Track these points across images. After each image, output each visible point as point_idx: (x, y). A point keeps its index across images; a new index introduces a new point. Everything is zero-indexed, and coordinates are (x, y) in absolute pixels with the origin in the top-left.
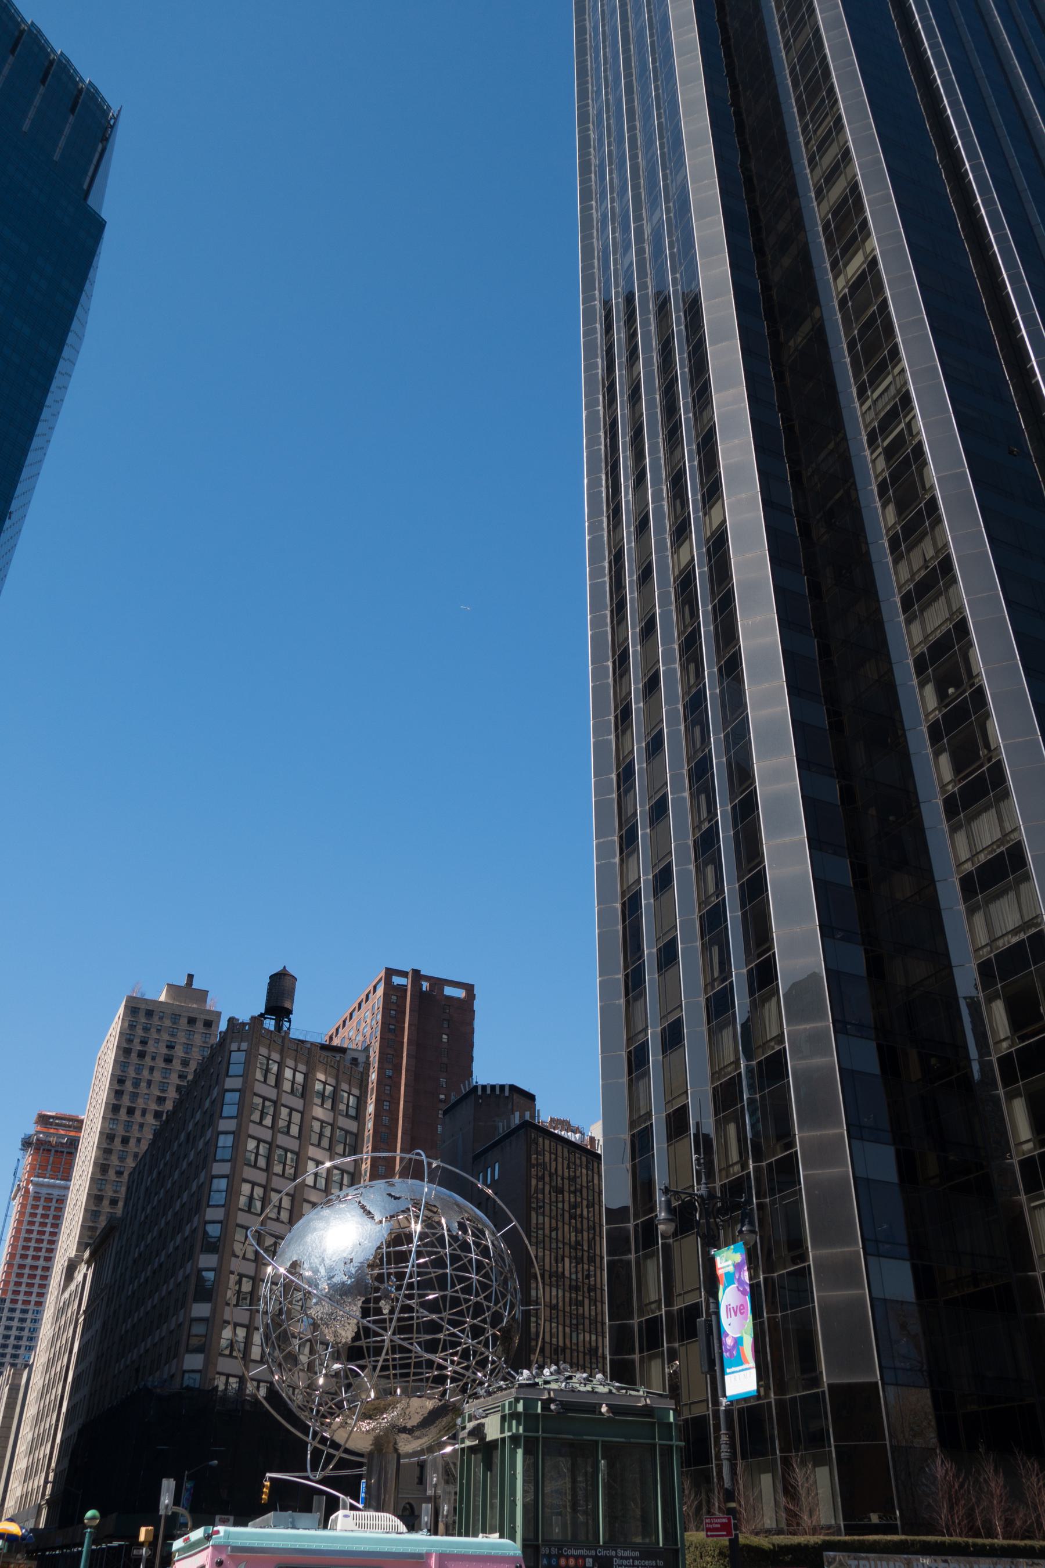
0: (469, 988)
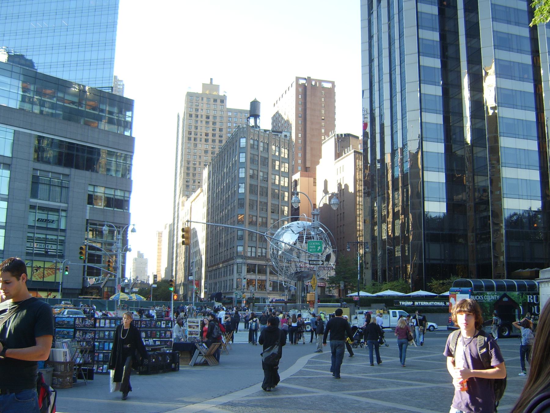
0: (333, 83)
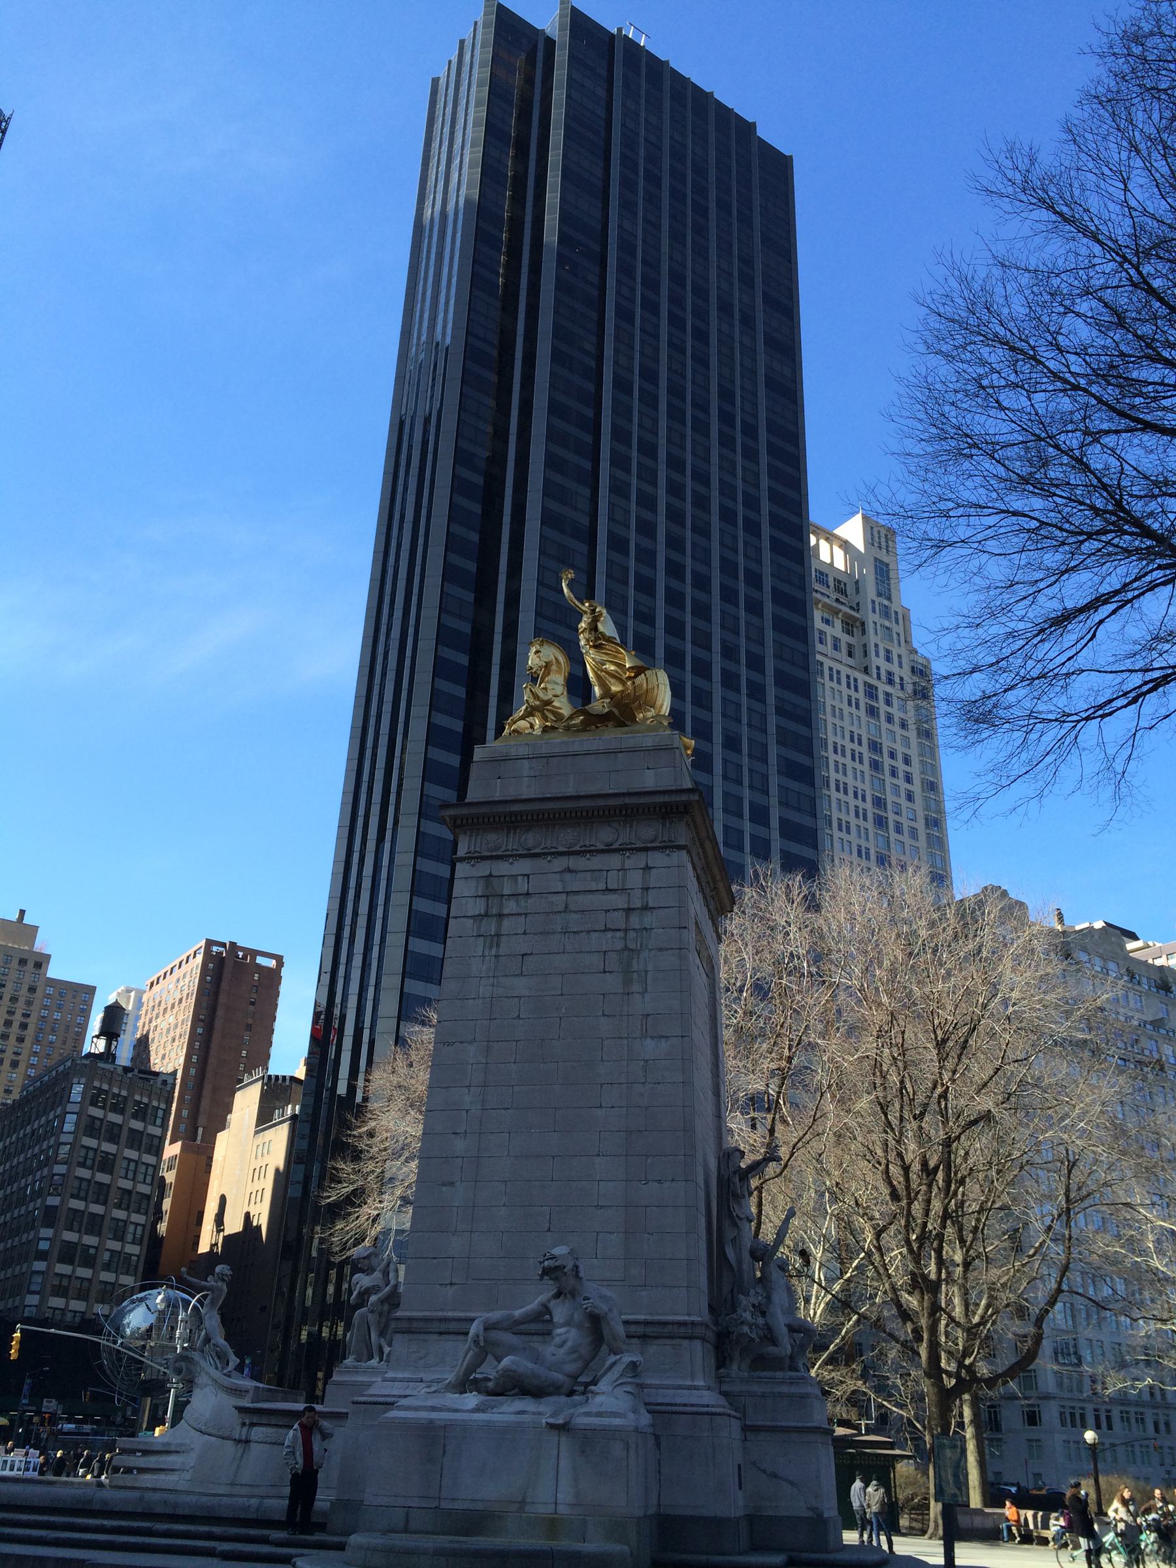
0: (279, 960)
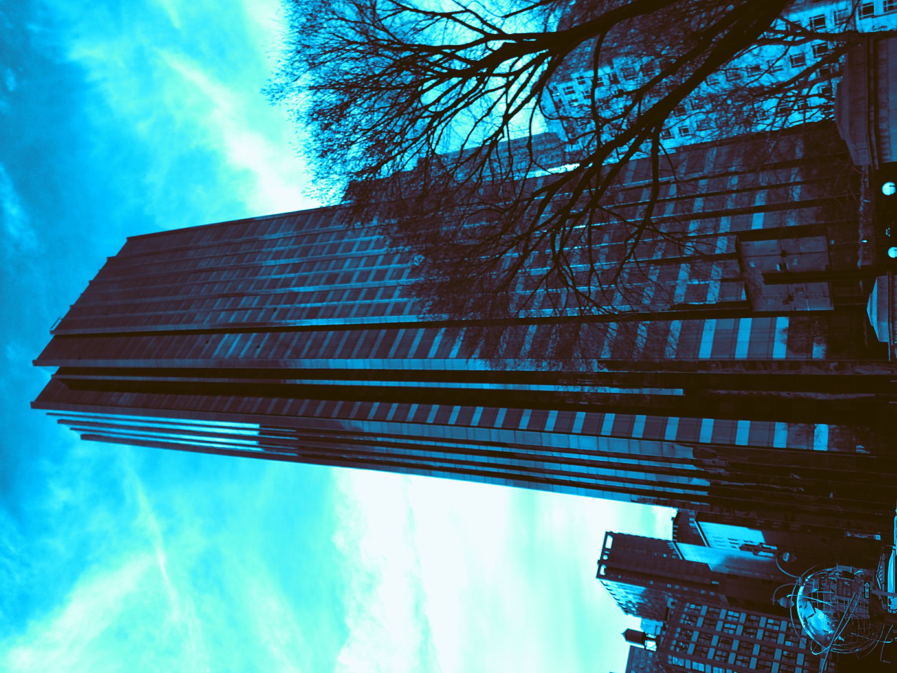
0: (607, 534)
